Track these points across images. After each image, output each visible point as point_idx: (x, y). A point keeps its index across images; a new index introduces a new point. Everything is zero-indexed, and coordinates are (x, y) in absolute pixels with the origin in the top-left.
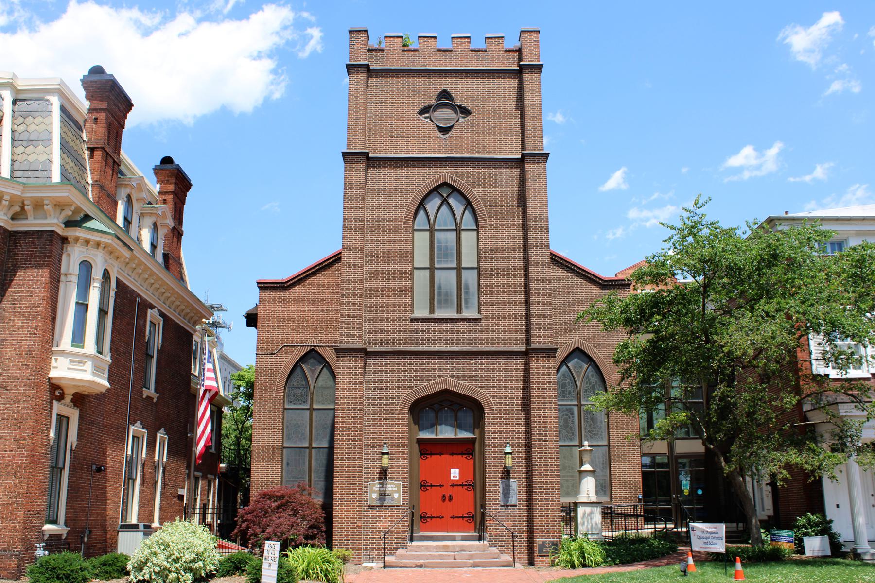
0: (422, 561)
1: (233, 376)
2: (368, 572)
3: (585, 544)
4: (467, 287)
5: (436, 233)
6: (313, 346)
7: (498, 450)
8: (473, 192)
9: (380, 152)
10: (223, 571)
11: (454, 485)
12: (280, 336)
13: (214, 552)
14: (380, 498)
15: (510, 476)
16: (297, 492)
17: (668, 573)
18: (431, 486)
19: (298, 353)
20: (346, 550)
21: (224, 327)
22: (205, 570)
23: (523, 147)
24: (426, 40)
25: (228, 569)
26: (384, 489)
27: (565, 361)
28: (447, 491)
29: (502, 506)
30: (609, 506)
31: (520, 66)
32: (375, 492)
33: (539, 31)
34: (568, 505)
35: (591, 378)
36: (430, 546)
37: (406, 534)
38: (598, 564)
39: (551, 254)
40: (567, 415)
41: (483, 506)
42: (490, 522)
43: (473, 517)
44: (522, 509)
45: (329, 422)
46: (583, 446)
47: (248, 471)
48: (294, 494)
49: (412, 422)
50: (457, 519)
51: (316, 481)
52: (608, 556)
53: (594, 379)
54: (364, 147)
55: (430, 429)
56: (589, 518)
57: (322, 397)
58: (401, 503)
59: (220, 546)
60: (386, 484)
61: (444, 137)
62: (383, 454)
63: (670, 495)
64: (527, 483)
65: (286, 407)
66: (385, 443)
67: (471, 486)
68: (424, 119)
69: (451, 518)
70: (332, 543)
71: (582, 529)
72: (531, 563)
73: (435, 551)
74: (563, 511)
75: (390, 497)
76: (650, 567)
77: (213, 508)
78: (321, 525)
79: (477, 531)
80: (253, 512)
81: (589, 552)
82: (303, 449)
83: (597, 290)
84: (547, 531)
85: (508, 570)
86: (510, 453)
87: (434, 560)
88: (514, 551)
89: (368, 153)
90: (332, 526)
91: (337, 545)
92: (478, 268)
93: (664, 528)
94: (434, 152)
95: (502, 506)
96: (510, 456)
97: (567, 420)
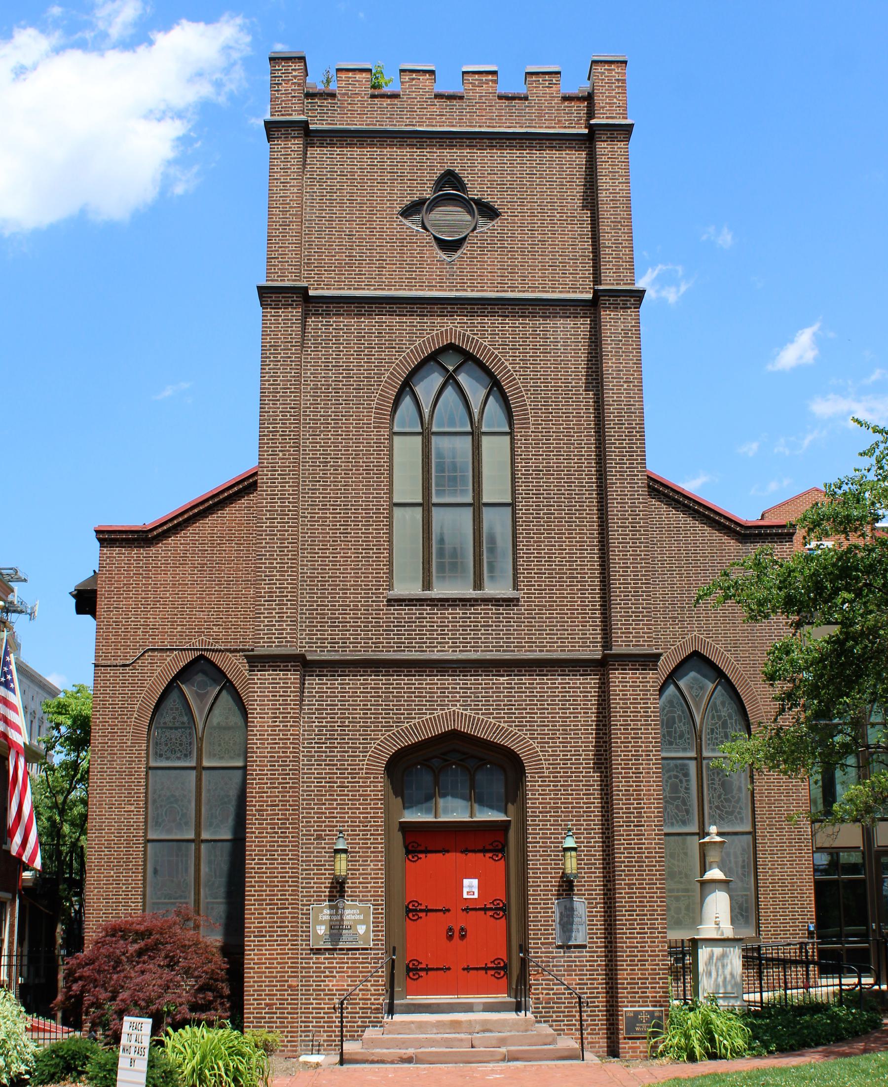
0: (411, 1051)
1: (48, 706)
2: (312, 1071)
3: (713, 1016)
4: (492, 540)
5: (434, 439)
6: (202, 650)
8: (500, 359)
9: (328, 286)
10: (42, 1074)
11: (470, 908)
12: (140, 632)
13: (24, 1038)
14: (331, 935)
15: (573, 890)
16: (175, 923)
17: (868, 1068)
18: (427, 911)
19: (175, 663)
20: (269, 1032)
21: (21, 612)
22: (9, 1073)
23: (597, 280)
24: (414, 76)
25: (52, 1070)
26: (339, 918)
27: (672, 677)
28: (458, 921)
29: (559, 947)
30: (755, 945)
31: (591, 127)
32: (322, 923)
33: (625, 62)
34: (680, 945)
35: (720, 707)
36: (426, 1023)
37: (381, 1001)
38: (737, 1053)
39: (648, 477)
40: (676, 777)
41: (524, 948)
43: (504, 968)
44: (597, 952)
45: (233, 793)
46: (708, 834)
47: (78, 886)
48: (170, 927)
49: (391, 791)
50: (475, 972)
51: (208, 903)
52: (755, 1037)
53: (727, 710)
54: (299, 278)
55: (424, 805)
56: (720, 964)
57: (220, 745)
58: (372, 943)
59: (33, 1029)
60: (343, 908)
61: (449, 259)
62: (337, 851)
63: (865, 922)
64: (604, 903)
65: (152, 764)
66: (341, 832)
67: (501, 910)
68: (412, 225)
69: (464, 969)
70: (243, 1018)
71: (706, 985)
72: (613, 1051)
73: (435, 1031)
74: (670, 954)
76: (832, 1057)
77: (10, 956)
78: (220, 985)
79: (513, 994)
80: (93, 963)
81: (722, 1031)
82: (185, 844)
83: (732, 544)
84: (642, 993)
85: (571, 1065)
86: (574, 849)
87: (433, 1049)
88: (581, 1030)
89: (306, 289)
90: (242, 987)
92: (512, 505)
93: (856, 986)
94: (431, 287)
95: (559, 947)
96: (574, 853)
97: (677, 786)
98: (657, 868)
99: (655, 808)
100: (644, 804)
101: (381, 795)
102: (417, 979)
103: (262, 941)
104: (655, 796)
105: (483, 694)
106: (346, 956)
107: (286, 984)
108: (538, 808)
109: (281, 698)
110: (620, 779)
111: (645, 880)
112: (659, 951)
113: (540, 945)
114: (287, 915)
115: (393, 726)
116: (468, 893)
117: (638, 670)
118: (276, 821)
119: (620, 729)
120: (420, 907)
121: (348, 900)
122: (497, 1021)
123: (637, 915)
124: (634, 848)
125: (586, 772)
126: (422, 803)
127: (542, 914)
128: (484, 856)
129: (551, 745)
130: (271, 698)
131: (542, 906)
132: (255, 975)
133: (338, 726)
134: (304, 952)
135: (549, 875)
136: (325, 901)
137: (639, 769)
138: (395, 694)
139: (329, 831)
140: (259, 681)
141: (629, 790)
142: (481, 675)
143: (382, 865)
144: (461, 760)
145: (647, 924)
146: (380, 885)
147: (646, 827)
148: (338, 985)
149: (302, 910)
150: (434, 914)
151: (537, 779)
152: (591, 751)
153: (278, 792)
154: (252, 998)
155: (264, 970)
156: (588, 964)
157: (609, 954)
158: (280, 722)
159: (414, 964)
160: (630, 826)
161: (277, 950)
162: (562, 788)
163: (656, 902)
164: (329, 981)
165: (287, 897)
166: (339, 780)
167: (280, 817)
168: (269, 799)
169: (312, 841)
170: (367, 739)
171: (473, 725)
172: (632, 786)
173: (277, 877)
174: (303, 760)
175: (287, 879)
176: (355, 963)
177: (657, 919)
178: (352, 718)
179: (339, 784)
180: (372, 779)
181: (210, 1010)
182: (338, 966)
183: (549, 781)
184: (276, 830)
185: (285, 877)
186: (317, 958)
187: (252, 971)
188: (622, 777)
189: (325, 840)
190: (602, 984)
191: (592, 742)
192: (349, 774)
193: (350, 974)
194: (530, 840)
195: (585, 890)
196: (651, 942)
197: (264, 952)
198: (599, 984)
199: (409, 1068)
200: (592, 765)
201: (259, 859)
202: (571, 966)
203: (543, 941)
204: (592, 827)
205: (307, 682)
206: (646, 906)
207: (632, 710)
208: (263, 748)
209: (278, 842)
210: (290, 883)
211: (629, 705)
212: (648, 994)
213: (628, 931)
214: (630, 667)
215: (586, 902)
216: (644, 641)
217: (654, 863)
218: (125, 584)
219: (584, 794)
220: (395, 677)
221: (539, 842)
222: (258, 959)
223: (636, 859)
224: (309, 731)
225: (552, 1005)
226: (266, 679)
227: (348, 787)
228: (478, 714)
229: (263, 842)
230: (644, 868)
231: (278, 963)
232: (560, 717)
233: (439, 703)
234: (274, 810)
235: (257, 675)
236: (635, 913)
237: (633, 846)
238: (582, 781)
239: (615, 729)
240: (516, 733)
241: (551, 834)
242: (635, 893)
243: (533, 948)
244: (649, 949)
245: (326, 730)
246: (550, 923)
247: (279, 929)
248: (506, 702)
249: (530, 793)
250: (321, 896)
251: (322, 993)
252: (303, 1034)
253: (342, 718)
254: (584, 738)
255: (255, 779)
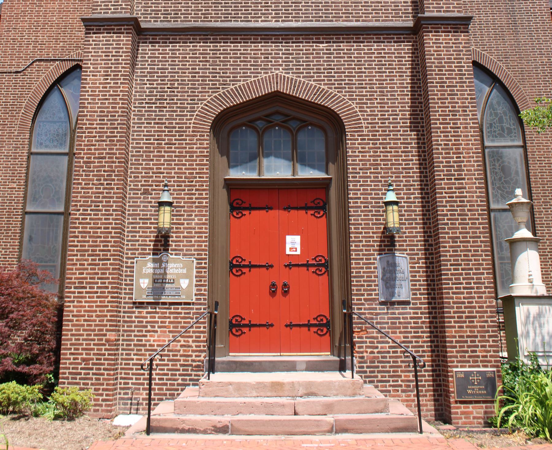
0: (226, 419)
6: (78, 60)
7: (372, 198)
12: (31, 47)
14: (154, 289)
15: (395, 246)
18: (251, 266)
26: (162, 271)
29: (382, 303)
32: (145, 276)
35: (496, 106)
36: (245, 384)
37: (202, 358)
41: (347, 304)
42: (361, 334)
43: (327, 325)
44: (420, 308)
46: (516, 196)
50: (298, 329)
53: (503, 108)
55: (249, 165)
58: (194, 298)
60: (167, 262)
62: (161, 204)
64: (426, 258)
73: (255, 394)
75: (174, 286)
79: (336, 352)
82: (56, 216)
84: (473, 351)
91: (67, 378)
95: (382, 303)
96: (395, 207)
98: (480, 221)
99: (475, 161)
100: (464, 157)
101: (207, 152)
102: (239, 335)
103: (82, 293)
104: (474, 150)
105: (304, 59)
106: (168, 311)
107: (104, 338)
108: (359, 165)
109: (113, 58)
110: (439, 134)
111: (469, 233)
112: (487, 307)
113: (363, 301)
114: (109, 266)
115: (219, 88)
116: (291, 249)
117: (450, 32)
118: (103, 173)
119: (436, 87)
120: (243, 263)
121: (172, 254)
122: (321, 384)
123: (463, 269)
124: (456, 202)
125: (404, 131)
126: (247, 163)
127: (365, 270)
128: (307, 213)
129: (369, 105)
130: (104, 58)
131: (364, 261)
132: (74, 328)
133: (168, 88)
134: (127, 306)
135: (371, 231)
136: (149, 254)
137: (456, 124)
138: (222, 59)
139: (156, 186)
140: (94, 43)
141: (448, 145)
142: (302, 42)
143: (206, 220)
144: (283, 122)
145: (473, 279)
146: (204, 239)
147: (466, 181)
148: (159, 341)
149: (127, 263)
150: (257, 270)
151: (356, 137)
152: (407, 111)
153: (106, 145)
154: (68, 352)
155: (82, 323)
156: (412, 321)
157: (434, 311)
158: (111, 79)
159: (236, 320)
160: (451, 179)
161: (96, 302)
162: (381, 146)
163: (481, 255)
164: (151, 336)
165: (109, 248)
166: (166, 138)
167: (106, 169)
168: (97, 152)
169: (139, 195)
170: (194, 100)
171: (295, 87)
172: (451, 140)
173: (100, 228)
174: (134, 119)
175: (110, 230)
176: (177, 318)
177: (483, 274)
178: (182, 80)
179: (166, 141)
180: (198, 137)
181: (36, 363)
182: (160, 320)
183: (368, 139)
184: (102, 182)
185: (108, 228)
186: (139, 312)
187: (70, 323)
188: (441, 132)
189: (152, 194)
190: (427, 342)
191: (408, 103)
192: (176, 132)
193: (171, 329)
194: (351, 196)
195: (407, 245)
196: (479, 297)
197: (83, 304)
198: (424, 342)
199: (222, 441)
200: (408, 124)
201: (84, 210)
202: (395, 323)
203: (366, 297)
204: (412, 183)
205: (140, 48)
206: (471, 260)
207: (447, 68)
208: (93, 103)
209: (103, 193)
210: (113, 235)
211: (443, 64)
212: (478, 354)
213: (454, 286)
214: (443, 29)
215: (408, 257)
216: (453, 7)
217: (477, 217)
218: (22, 11)
219: (402, 152)
220: (222, 44)
221: (360, 198)
222: (77, 311)
223: (459, 212)
224: (141, 92)
225: (376, 364)
226: (100, 41)
227: (175, 144)
228: (300, 77)
229: (89, 193)
230: (467, 221)
231: (97, 316)
232: (376, 80)
233: (263, 67)
234: (101, 162)
235: (92, 37)
236: (460, 267)
237: (454, 199)
238: (400, 139)
239: (431, 87)
240: (336, 95)
241: (371, 190)
242: (459, 246)
243: (356, 304)
244: (477, 305)
245: (157, 92)
246: (373, 279)
247: (100, 281)
248: (326, 67)
249: (350, 151)
250: (145, 249)
251: (143, 348)
252: (122, 392)
253: (172, 81)
254: (401, 99)
255: (84, 132)
